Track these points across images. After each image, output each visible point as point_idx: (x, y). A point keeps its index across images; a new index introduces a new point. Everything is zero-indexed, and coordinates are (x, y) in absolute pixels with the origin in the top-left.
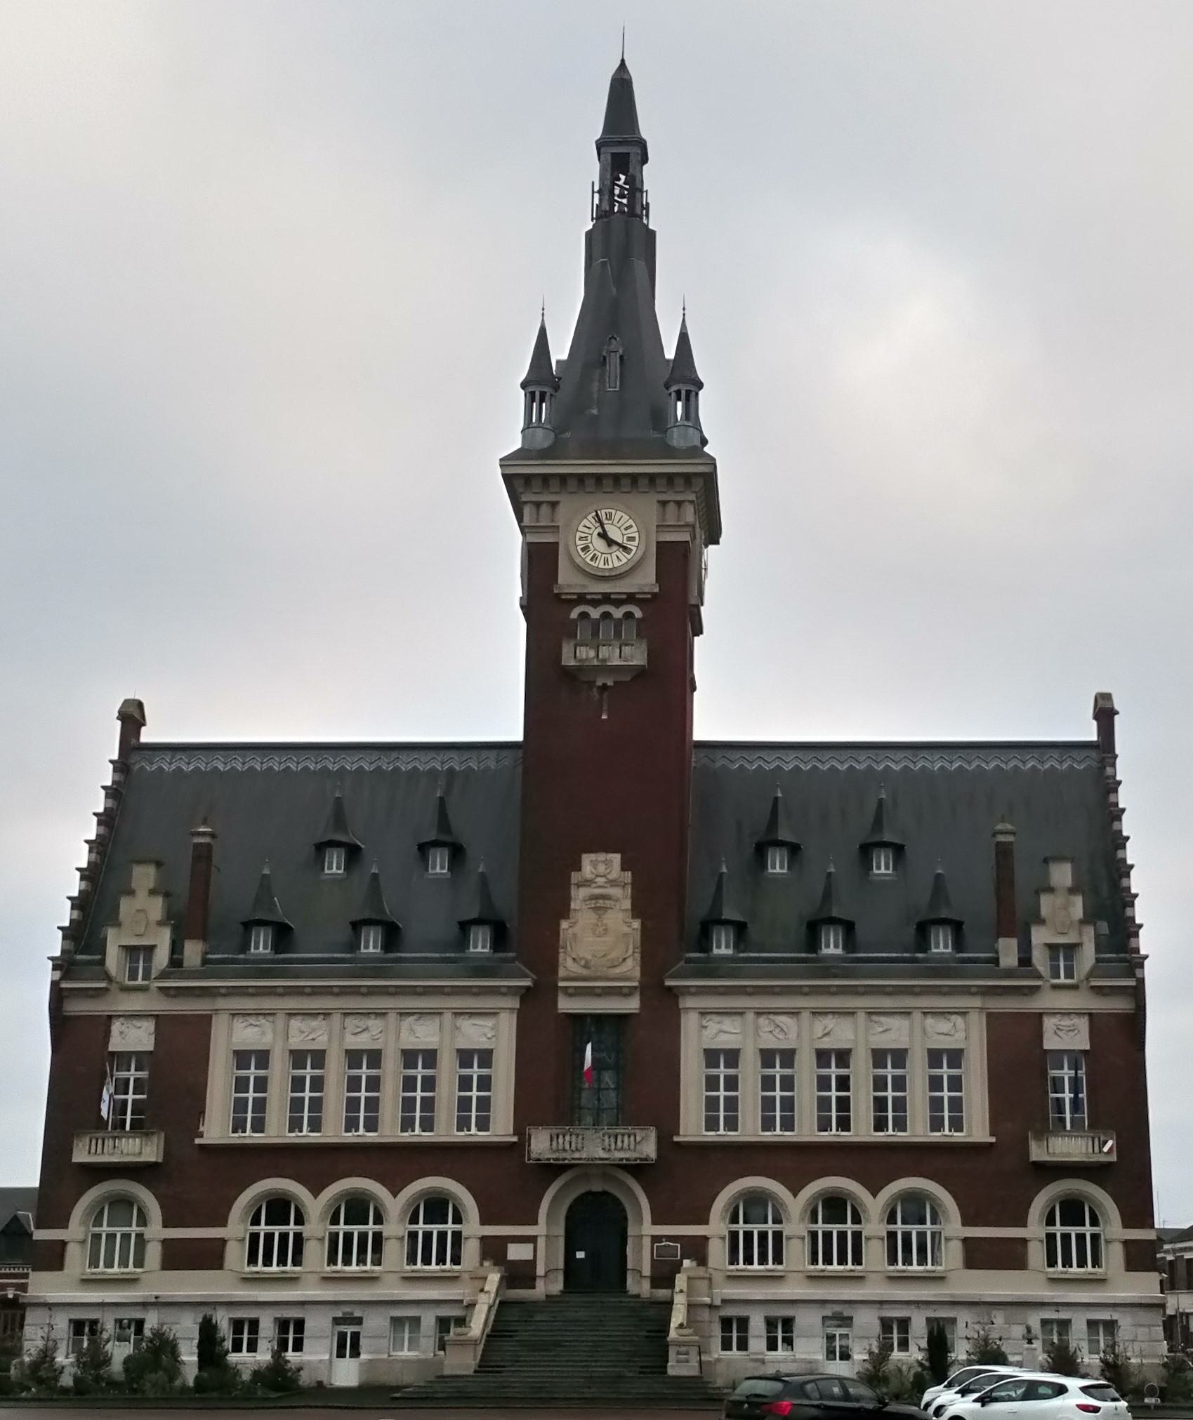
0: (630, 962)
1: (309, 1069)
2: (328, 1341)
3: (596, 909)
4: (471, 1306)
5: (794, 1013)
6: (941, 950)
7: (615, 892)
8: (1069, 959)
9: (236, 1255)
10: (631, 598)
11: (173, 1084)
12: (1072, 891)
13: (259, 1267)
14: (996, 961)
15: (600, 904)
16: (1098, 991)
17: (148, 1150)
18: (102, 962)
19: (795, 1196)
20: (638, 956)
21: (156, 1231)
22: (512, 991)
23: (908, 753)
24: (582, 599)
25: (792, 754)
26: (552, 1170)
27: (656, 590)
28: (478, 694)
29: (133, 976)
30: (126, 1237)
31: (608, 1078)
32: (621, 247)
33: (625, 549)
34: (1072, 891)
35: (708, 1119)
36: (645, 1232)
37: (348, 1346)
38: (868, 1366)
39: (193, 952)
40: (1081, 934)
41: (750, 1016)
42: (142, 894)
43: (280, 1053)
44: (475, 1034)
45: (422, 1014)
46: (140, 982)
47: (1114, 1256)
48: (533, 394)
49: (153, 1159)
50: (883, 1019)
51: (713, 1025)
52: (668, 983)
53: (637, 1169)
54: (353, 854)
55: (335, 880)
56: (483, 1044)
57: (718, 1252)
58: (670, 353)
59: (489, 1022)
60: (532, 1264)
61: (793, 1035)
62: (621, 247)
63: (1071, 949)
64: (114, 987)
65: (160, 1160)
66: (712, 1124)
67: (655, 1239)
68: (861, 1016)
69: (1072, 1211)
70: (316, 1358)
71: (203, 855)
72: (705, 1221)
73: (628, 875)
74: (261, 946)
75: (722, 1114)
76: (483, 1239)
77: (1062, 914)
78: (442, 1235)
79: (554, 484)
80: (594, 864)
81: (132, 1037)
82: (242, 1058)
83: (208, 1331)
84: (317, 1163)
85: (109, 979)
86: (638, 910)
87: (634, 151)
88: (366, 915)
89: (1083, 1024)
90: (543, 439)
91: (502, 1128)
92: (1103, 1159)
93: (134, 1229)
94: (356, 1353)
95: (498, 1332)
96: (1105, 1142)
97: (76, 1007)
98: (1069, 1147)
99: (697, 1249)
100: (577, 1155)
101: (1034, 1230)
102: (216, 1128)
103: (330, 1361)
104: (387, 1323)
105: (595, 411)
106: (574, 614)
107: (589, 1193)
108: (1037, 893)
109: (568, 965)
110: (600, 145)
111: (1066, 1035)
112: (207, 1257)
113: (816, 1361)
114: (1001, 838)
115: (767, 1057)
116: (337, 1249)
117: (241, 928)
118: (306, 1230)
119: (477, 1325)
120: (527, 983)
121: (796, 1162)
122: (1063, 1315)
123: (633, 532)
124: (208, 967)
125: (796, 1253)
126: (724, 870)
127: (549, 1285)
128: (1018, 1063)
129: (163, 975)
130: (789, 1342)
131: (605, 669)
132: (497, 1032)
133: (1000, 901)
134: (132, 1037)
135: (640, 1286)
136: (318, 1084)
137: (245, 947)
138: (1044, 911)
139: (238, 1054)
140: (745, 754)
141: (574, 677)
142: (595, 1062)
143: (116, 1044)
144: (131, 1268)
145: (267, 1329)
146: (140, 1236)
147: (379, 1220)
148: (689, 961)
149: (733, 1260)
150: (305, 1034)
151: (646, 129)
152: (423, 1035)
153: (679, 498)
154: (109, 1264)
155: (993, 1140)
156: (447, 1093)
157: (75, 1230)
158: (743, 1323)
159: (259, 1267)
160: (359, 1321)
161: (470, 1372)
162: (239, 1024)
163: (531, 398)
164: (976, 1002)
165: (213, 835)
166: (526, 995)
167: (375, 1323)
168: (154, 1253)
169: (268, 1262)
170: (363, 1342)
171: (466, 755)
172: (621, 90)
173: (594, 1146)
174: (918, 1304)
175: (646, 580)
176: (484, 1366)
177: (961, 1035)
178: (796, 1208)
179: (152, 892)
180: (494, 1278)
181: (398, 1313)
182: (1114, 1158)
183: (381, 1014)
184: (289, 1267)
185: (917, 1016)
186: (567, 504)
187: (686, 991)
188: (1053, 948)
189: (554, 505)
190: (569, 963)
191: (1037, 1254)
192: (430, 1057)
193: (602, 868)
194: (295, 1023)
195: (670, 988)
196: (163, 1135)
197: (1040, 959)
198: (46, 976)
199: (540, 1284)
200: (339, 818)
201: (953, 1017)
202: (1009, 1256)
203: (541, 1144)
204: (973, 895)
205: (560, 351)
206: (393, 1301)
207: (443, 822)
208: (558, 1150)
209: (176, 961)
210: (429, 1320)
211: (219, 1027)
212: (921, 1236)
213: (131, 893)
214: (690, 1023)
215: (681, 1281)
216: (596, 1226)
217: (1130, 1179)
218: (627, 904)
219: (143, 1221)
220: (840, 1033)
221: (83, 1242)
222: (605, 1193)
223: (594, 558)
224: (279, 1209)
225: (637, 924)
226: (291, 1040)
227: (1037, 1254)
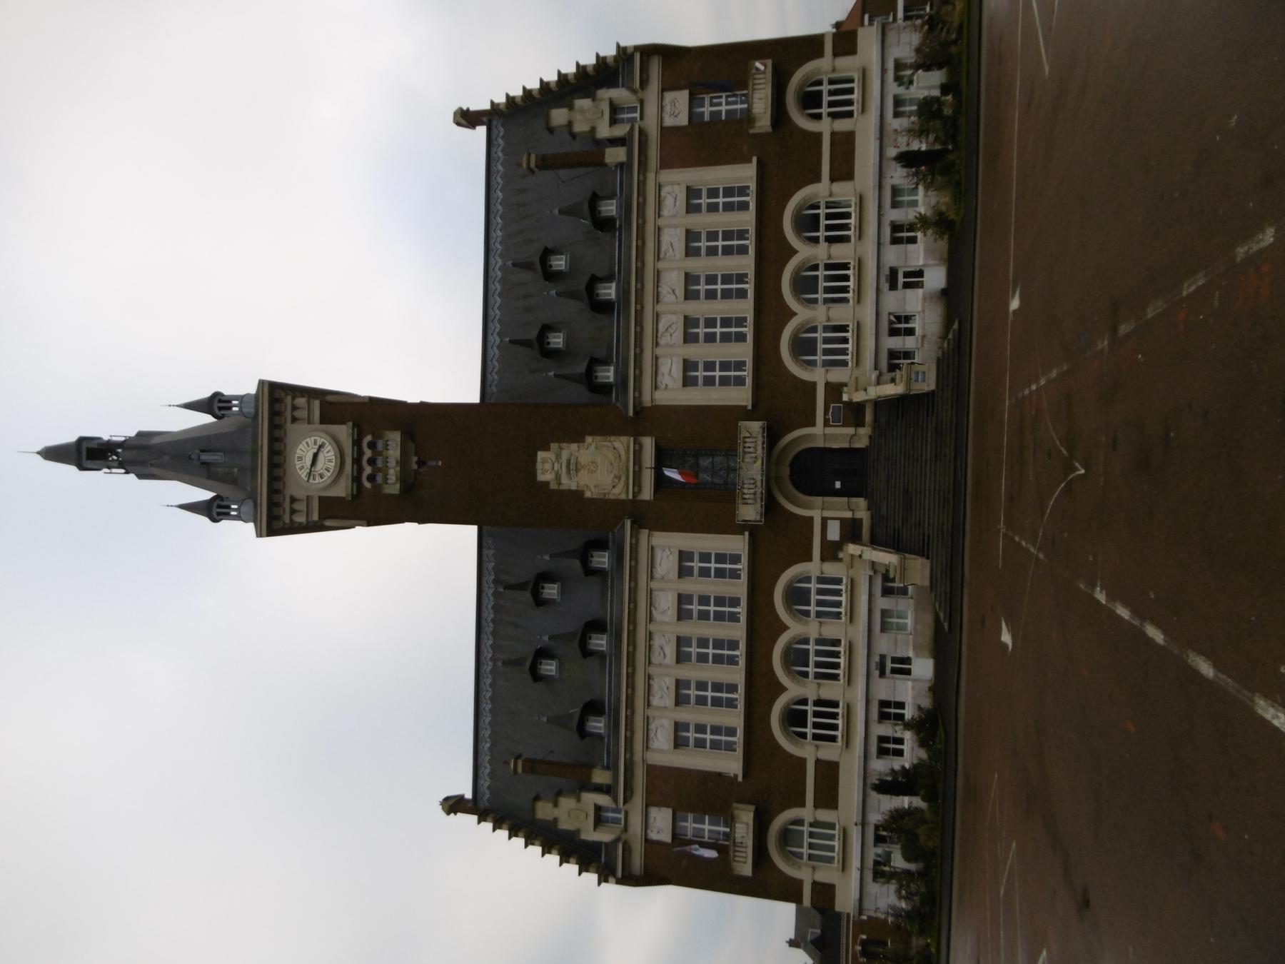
0: (617, 444)
1: (690, 692)
2: (898, 682)
3: (577, 470)
4: (873, 565)
5: (657, 317)
6: (614, 208)
8: (622, 110)
9: (829, 752)
10: (357, 443)
11: (703, 794)
12: (571, 107)
13: (839, 733)
14: (621, 165)
15: (573, 467)
16: (644, 83)
17: (745, 818)
18: (607, 844)
19: (795, 314)
20: (612, 438)
21: (807, 813)
22: (635, 535)
23: (492, 254)
24: (357, 479)
25: (490, 338)
26: (771, 506)
27: (350, 424)
28: (431, 566)
29: (616, 821)
30: (811, 835)
32: (144, 456)
33: (321, 446)
34: (571, 107)
35: (736, 384)
36: (822, 433)
37: (902, 667)
38: (930, 232)
39: (600, 777)
40: (602, 100)
41: (659, 351)
43: (678, 712)
44: (666, 564)
46: (622, 816)
47: (847, 65)
48: (219, 514)
49: (751, 815)
50: (663, 249)
51: (665, 379)
52: (631, 413)
53: (772, 437)
54: (543, 654)
55: (560, 668)
56: (674, 559)
57: (837, 375)
58: (207, 419)
59: (659, 553)
60: (843, 521)
61: (674, 318)
62: (144, 456)
63: (615, 109)
64: (624, 837)
65: (753, 808)
66: (740, 381)
67: (826, 424)
68: (660, 265)
69: (810, 100)
70: (911, 692)
71: (532, 766)
72: (814, 385)
73: (554, 446)
74: (597, 725)
75: (732, 373)
76: (823, 559)
77: (588, 115)
79: (276, 498)
80: (544, 472)
81: (661, 824)
82: (679, 743)
83: (887, 787)
85: (617, 840)
86: (578, 438)
87: (85, 445)
88: (576, 644)
89: (669, 96)
90: (248, 508)
91: (738, 544)
92: (770, 70)
93: (806, 829)
94: (907, 660)
96: (757, 69)
98: (761, 103)
99: (834, 390)
100: (759, 484)
101: (825, 127)
102: (731, 765)
103: (914, 680)
104: (885, 635)
105: (236, 470)
106: (368, 485)
107: (791, 476)
108: (574, 136)
109: (619, 492)
111: (677, 108)
113: (924, 294)
114: (533, 164)
115: (689, 338)
116: (828, 673)
117: (587, 739)
118: (812, 698)
119: (887, 558)
120: (628, 523)
121: (770, 314)
122: (890, 66)
123: (310, 440)
124: (612, 767)
126: (552, 374)
127: (860, 509)
128: (701, 143)
129: (615, 800)
130: (907, 319)
131: (403, 462)
132: (665, 548)
133: (580, 164)
134: (661, 824)
135: (862, 437)
136: (702, 686)
137: (600, 737)
138: (586, 128)
139: (677, 746)
140: (489, 370)
141: (409, 485)
143: (666, 837)
144: (836, 832)
145: (886, 729)
146: (811, 825)
148: (617, 399)
150: (663, 695)
151: (71, 438)
152: (666, 604)
153: (289, 408)
154: (831, 849)
155: (755, 159)
157: (804, 875)
159: (839, 733)
160: (883, 657)
161: (927, 563)
162: (655, 744)
163: (227, 515)
164: (651, 176)
165: (517, 758)
166: (638, 524)
167: (884, 645)
168: (824, 815)
169: (835, 727)
170: (899, 654)
171: (485, 571)
172: (54, 454)
173: (752, 470)
174: (880, 215)
175: (344, 432)
176: (922, 552)
177: (676, 188)
178: (806, 314)
179: (556, 804)
180: (852, 549)
182: (769, 62)
183: (650, 636)
184: (839, 710)
185: (661, 222)
186: (292, 490)
187: (638, 400)
188: (613, 121)
189: (293, 500)
190: (616, 491)
191: (842, 125)
192: (683, 599)
193: (548, 466)
194: (655, 701)
195: (636, 412)
196: (735, 805)
198: (611, 888)
199: (859, 515)
200: (517, 663)
201: (663, 194)
202: (845, 146)
203: (750, 512)
206: (869, 631)
207: (520, 587)
208: (755, 499)
210: (883, 603)
211: (656, 759)
212: (829, 216)
213: (556, 820)
215: (859, 397)
216: (815, 471)
217: (788, 53)
218: (574, 446)
219: (800, 822)
220: (673, 281)
221: (814, 868)
222: (792, 464)
223: (327, 470)
224: (795, 718)
225: (589, 439)
226: (668, 704)
227: (842, 125)
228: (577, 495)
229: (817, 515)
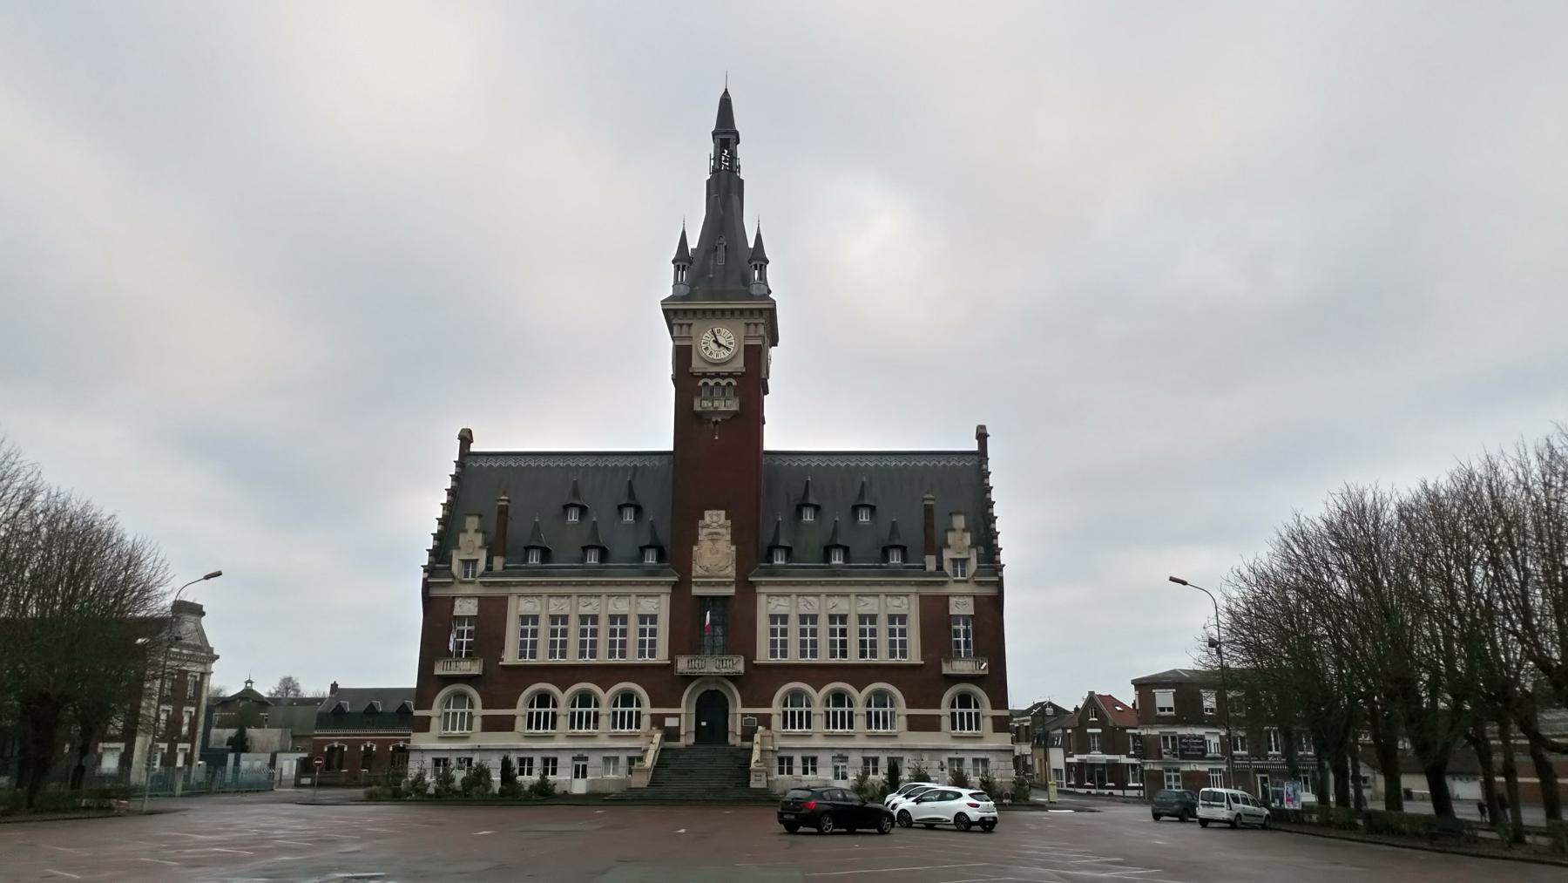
4: (646, 751)
5: (817, 595)
7: (722, 531)
9: (521, 724)
10: (730, 375)
15: (714, 537)
16: (979, 583)
17: (473, 668)
21: (478, 711)
24: (704, 375)
26: (688, 679)
29: (466, 575)
30: (462, 714)
31: (718, 630)
32: (725, 188)
36: (738, 712)
37: (580, 772)
42: (471, 531)
43: (547, 616)
44: (647, 606)
45: (620, 596)
47: (987, 724)
51: (774, 601)
53: (734, 678)
54: (583, 510)
55: (573, 525)
56: (652, 611)
57: (777, 722)
58: (751, 245)
62: (725, 188)
66: (773, 654)
67: (744, 715)
69: (965, 700)
70: (563, 778)
71: (503, 512)
74: (534, 560)
77: (959, 543)
78: (546, 714)
81: (466, 608)
84: (564, 675)
86: (734, 541)
87: (732, 137)
89: (971, 601)
90: (684, 290)
91: (662, 656)
93: (467, 710)
94: (584, 776)
95: (660, 764)
97: (436, 592)
99: (766, 721)
101: (945, 710)
102: (510, 657)
109: (697, 570)
110: (714, 134)
111: (961, 607)
112: (507, 725)
119: (649, 761)
125: (818, 723)
127: (687, 740)
128: (936, 621)
129: (482, 575)
130: (814, 770)
132: (659, 605)
134: (466, 608)
135: (735, 740)
137: (526, 560)
141: (700, 417)
142: (712, 621)
143: (457, 612)
145: (538, 763)
147: (597, 705)
149: (785, 726)
150: (557, 606)
152: (620, 607)
156: (633, 638)
157: (436, 711)
158: (790, 760)
160: (586, 759)
162: (522, 601)
164: (914, 589)
166: (675, 586)
167: (595, 760)
168: (477, 723)
173: (711, 666)
180: (658, 736)
181: (607, 754)
183: (598, 596)
186: (697, 324)
188: (954, 561)
189: (690, 325)
191: (946, 723)
192: (624, 619)
197: (947, 566)
200: (576, 492)
202: (932, 725)
203: (683, 665)
204: (912, 532)
205: (693, 244)
209: (489, 568)
210: (623, 758)
211: (512, 603)
213: (465, 531)
214: (762, 601)
215: (757, 737)
216: (712, 708)
217: (996, 683)
219: (472, 706)
220: (842, 606)
228: (695, 541)
229: (682, 710)
